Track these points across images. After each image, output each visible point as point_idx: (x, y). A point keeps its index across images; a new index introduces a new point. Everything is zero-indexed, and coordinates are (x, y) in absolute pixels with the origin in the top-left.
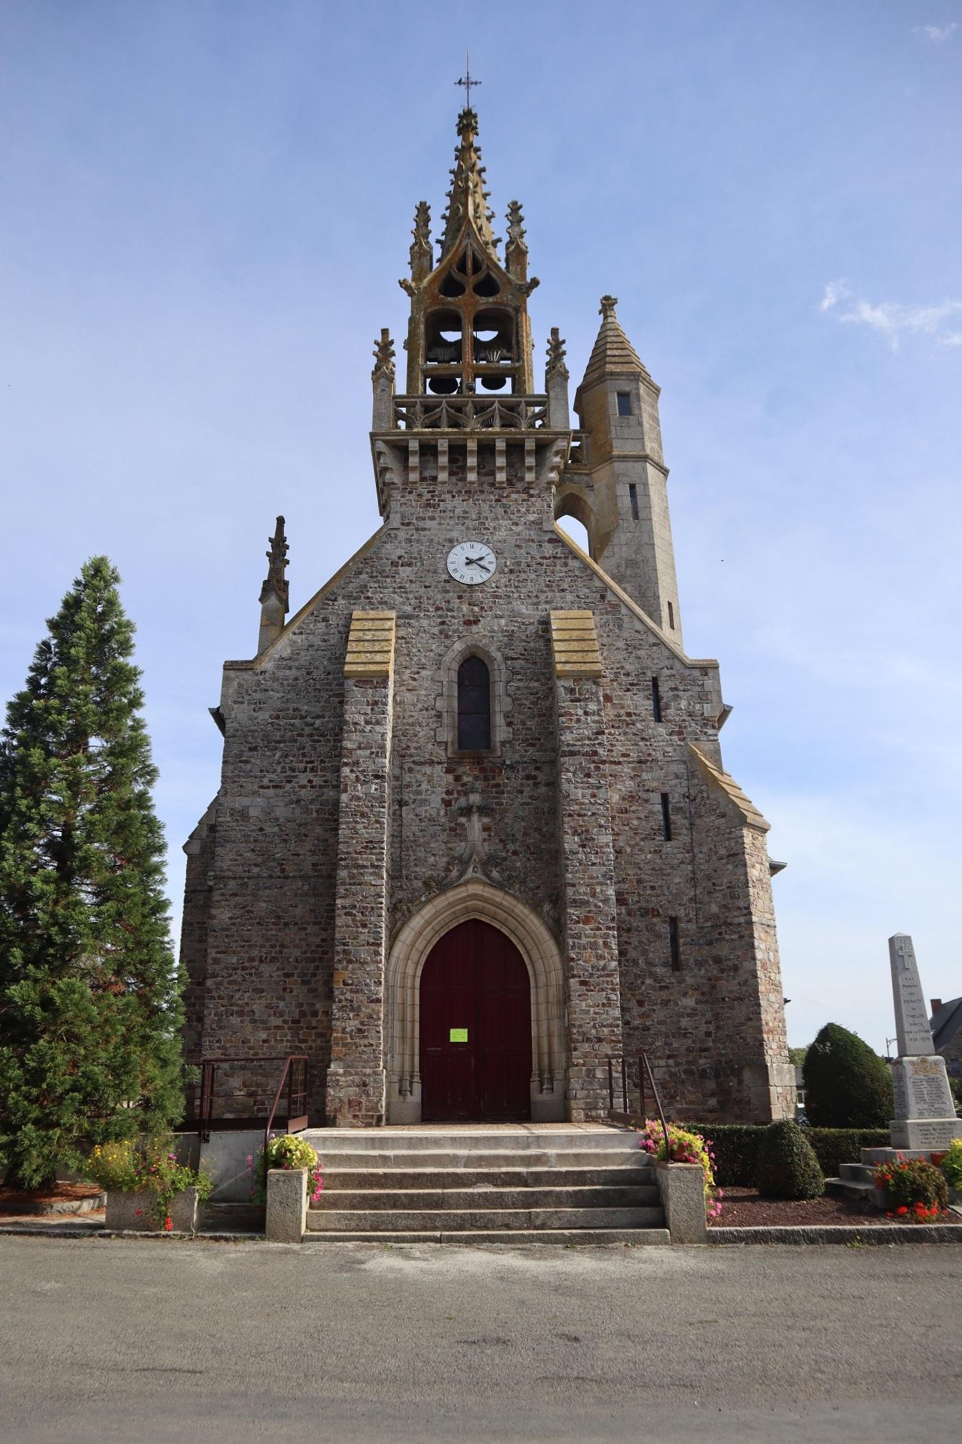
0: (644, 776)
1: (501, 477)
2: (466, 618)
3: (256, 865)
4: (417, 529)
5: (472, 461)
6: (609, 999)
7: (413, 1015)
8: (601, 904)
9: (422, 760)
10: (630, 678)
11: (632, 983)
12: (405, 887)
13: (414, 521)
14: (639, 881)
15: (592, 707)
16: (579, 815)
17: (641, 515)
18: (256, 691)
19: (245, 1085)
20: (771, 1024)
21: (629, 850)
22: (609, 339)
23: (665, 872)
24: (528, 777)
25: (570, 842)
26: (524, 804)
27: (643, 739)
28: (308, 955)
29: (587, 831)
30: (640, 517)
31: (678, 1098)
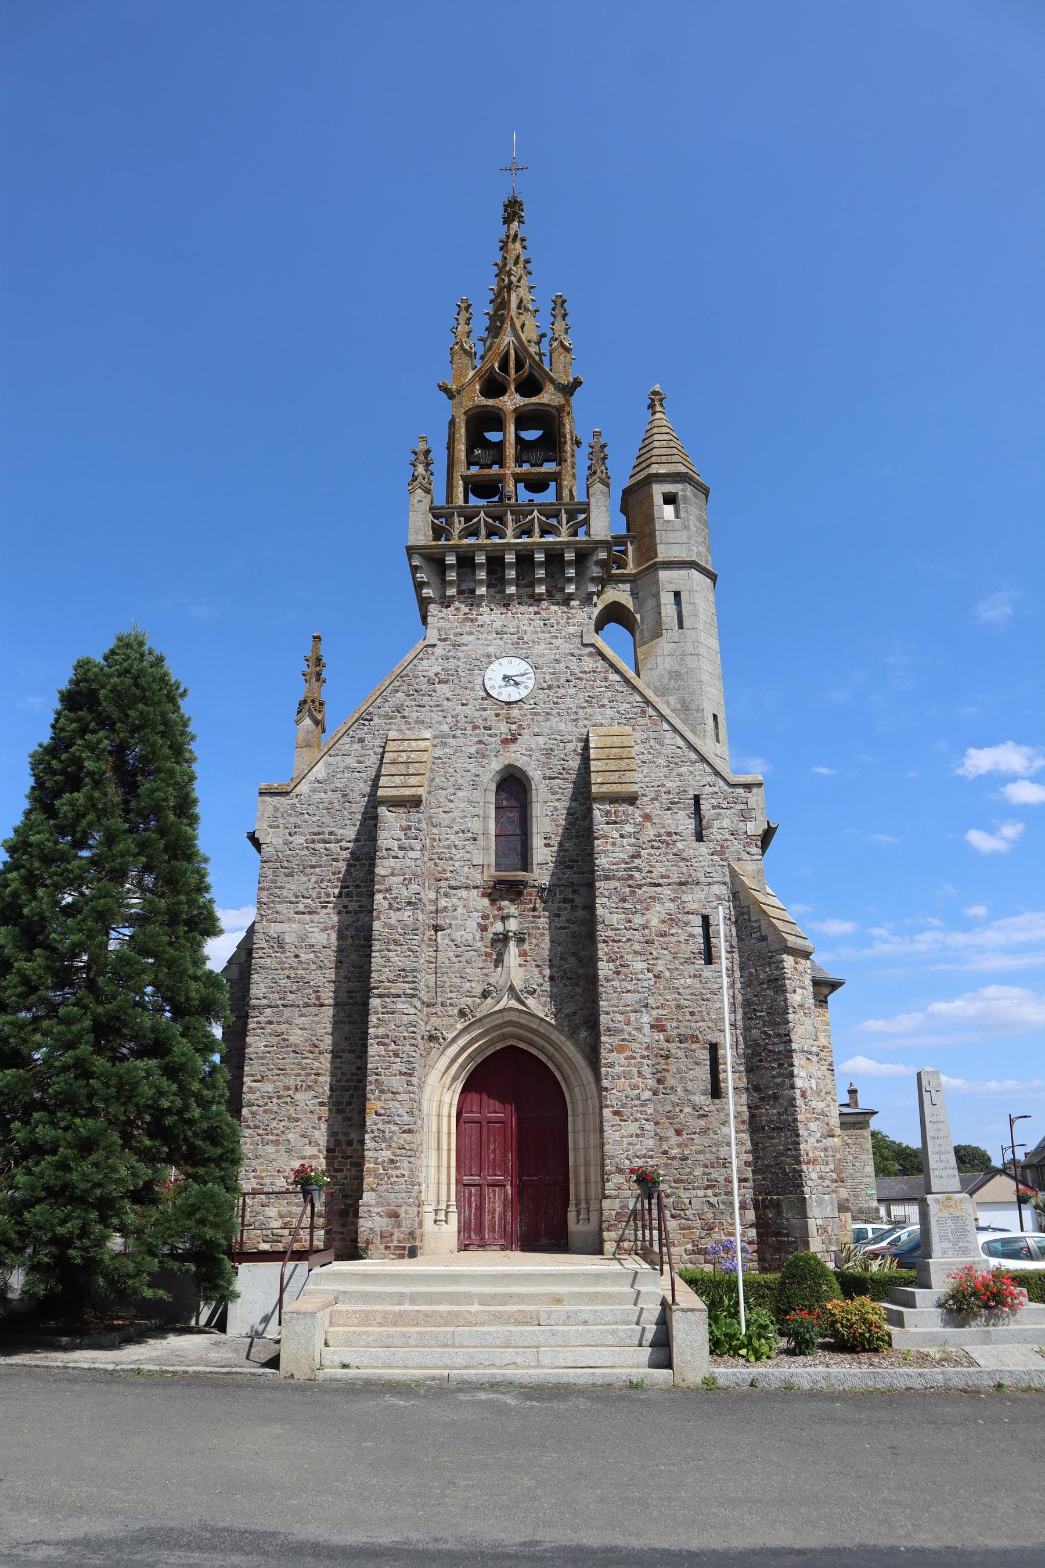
0: (685, 898)
1: (541, 589)
2: (503, 736)
3: (291, 992)
4: (454, 645)
5: (511, 574)
6: (642, 1129)
7: (449, 1144)
8: (634, 1032)
9: (458, 884)
10: (671, 796)
11: (670, 1112)
12: (440, 1013)
13: (452, 636)
14: (678, 1007)
15: (629, 829)
16: (614, 941)
17: (687, 623)
18: (290, 815)
19: (281, 1216)
20: (811, 1154)
21: (668, 974)
22: (655, 452)
23: (705, 997)
24: (565, 901)
25: (604, 969)
26: (561, 928)
27: (684, 859)
28: (343, 1083)
29: (622, 957)
30: (685, 626)
31: (716, 1229)
